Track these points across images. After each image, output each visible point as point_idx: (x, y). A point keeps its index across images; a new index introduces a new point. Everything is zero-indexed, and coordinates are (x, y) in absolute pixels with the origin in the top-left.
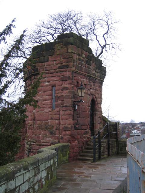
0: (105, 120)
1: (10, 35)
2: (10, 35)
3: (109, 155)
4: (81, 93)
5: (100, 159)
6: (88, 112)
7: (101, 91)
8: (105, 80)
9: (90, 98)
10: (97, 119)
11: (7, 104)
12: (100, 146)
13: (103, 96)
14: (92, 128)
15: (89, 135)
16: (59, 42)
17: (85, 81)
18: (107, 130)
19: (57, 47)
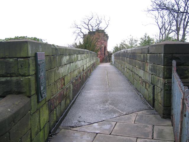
0: (108, 52)
1: (117, 74)
2: (117, 74)
3: (109, 62)
4: (102, 45)
5: (107, 62)
6: (104, 50)
7: (107, 43)
8: (108, 40)
9: (104, 46)
10: (106, 52)
11: (144, 83)
12: (107, 59)
13: (108, 45)
14: (105, 54)
15: (104, 56)
16: (96, 32)
17: (103, 41)
18: (109, 55)
19: (96, 33)
